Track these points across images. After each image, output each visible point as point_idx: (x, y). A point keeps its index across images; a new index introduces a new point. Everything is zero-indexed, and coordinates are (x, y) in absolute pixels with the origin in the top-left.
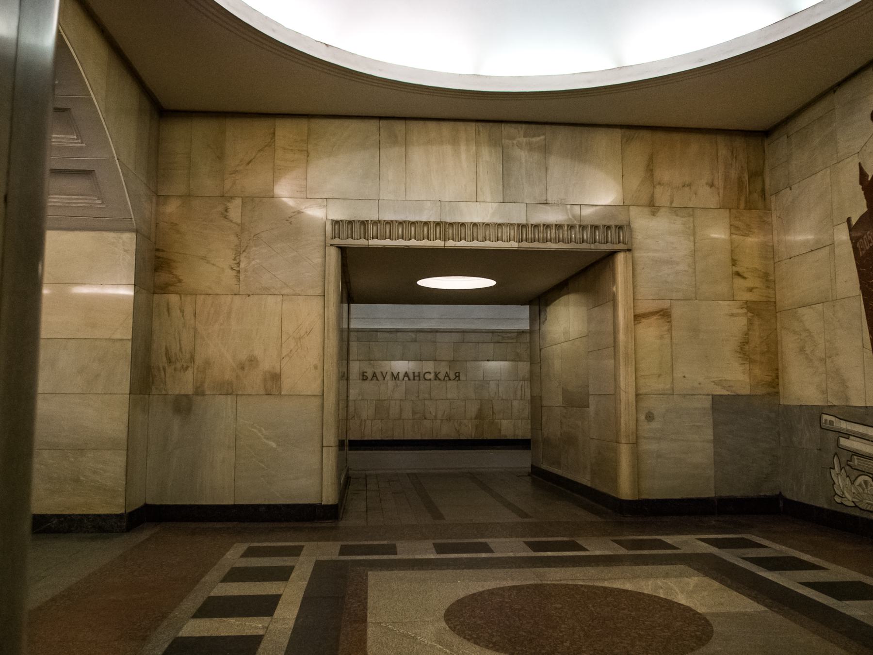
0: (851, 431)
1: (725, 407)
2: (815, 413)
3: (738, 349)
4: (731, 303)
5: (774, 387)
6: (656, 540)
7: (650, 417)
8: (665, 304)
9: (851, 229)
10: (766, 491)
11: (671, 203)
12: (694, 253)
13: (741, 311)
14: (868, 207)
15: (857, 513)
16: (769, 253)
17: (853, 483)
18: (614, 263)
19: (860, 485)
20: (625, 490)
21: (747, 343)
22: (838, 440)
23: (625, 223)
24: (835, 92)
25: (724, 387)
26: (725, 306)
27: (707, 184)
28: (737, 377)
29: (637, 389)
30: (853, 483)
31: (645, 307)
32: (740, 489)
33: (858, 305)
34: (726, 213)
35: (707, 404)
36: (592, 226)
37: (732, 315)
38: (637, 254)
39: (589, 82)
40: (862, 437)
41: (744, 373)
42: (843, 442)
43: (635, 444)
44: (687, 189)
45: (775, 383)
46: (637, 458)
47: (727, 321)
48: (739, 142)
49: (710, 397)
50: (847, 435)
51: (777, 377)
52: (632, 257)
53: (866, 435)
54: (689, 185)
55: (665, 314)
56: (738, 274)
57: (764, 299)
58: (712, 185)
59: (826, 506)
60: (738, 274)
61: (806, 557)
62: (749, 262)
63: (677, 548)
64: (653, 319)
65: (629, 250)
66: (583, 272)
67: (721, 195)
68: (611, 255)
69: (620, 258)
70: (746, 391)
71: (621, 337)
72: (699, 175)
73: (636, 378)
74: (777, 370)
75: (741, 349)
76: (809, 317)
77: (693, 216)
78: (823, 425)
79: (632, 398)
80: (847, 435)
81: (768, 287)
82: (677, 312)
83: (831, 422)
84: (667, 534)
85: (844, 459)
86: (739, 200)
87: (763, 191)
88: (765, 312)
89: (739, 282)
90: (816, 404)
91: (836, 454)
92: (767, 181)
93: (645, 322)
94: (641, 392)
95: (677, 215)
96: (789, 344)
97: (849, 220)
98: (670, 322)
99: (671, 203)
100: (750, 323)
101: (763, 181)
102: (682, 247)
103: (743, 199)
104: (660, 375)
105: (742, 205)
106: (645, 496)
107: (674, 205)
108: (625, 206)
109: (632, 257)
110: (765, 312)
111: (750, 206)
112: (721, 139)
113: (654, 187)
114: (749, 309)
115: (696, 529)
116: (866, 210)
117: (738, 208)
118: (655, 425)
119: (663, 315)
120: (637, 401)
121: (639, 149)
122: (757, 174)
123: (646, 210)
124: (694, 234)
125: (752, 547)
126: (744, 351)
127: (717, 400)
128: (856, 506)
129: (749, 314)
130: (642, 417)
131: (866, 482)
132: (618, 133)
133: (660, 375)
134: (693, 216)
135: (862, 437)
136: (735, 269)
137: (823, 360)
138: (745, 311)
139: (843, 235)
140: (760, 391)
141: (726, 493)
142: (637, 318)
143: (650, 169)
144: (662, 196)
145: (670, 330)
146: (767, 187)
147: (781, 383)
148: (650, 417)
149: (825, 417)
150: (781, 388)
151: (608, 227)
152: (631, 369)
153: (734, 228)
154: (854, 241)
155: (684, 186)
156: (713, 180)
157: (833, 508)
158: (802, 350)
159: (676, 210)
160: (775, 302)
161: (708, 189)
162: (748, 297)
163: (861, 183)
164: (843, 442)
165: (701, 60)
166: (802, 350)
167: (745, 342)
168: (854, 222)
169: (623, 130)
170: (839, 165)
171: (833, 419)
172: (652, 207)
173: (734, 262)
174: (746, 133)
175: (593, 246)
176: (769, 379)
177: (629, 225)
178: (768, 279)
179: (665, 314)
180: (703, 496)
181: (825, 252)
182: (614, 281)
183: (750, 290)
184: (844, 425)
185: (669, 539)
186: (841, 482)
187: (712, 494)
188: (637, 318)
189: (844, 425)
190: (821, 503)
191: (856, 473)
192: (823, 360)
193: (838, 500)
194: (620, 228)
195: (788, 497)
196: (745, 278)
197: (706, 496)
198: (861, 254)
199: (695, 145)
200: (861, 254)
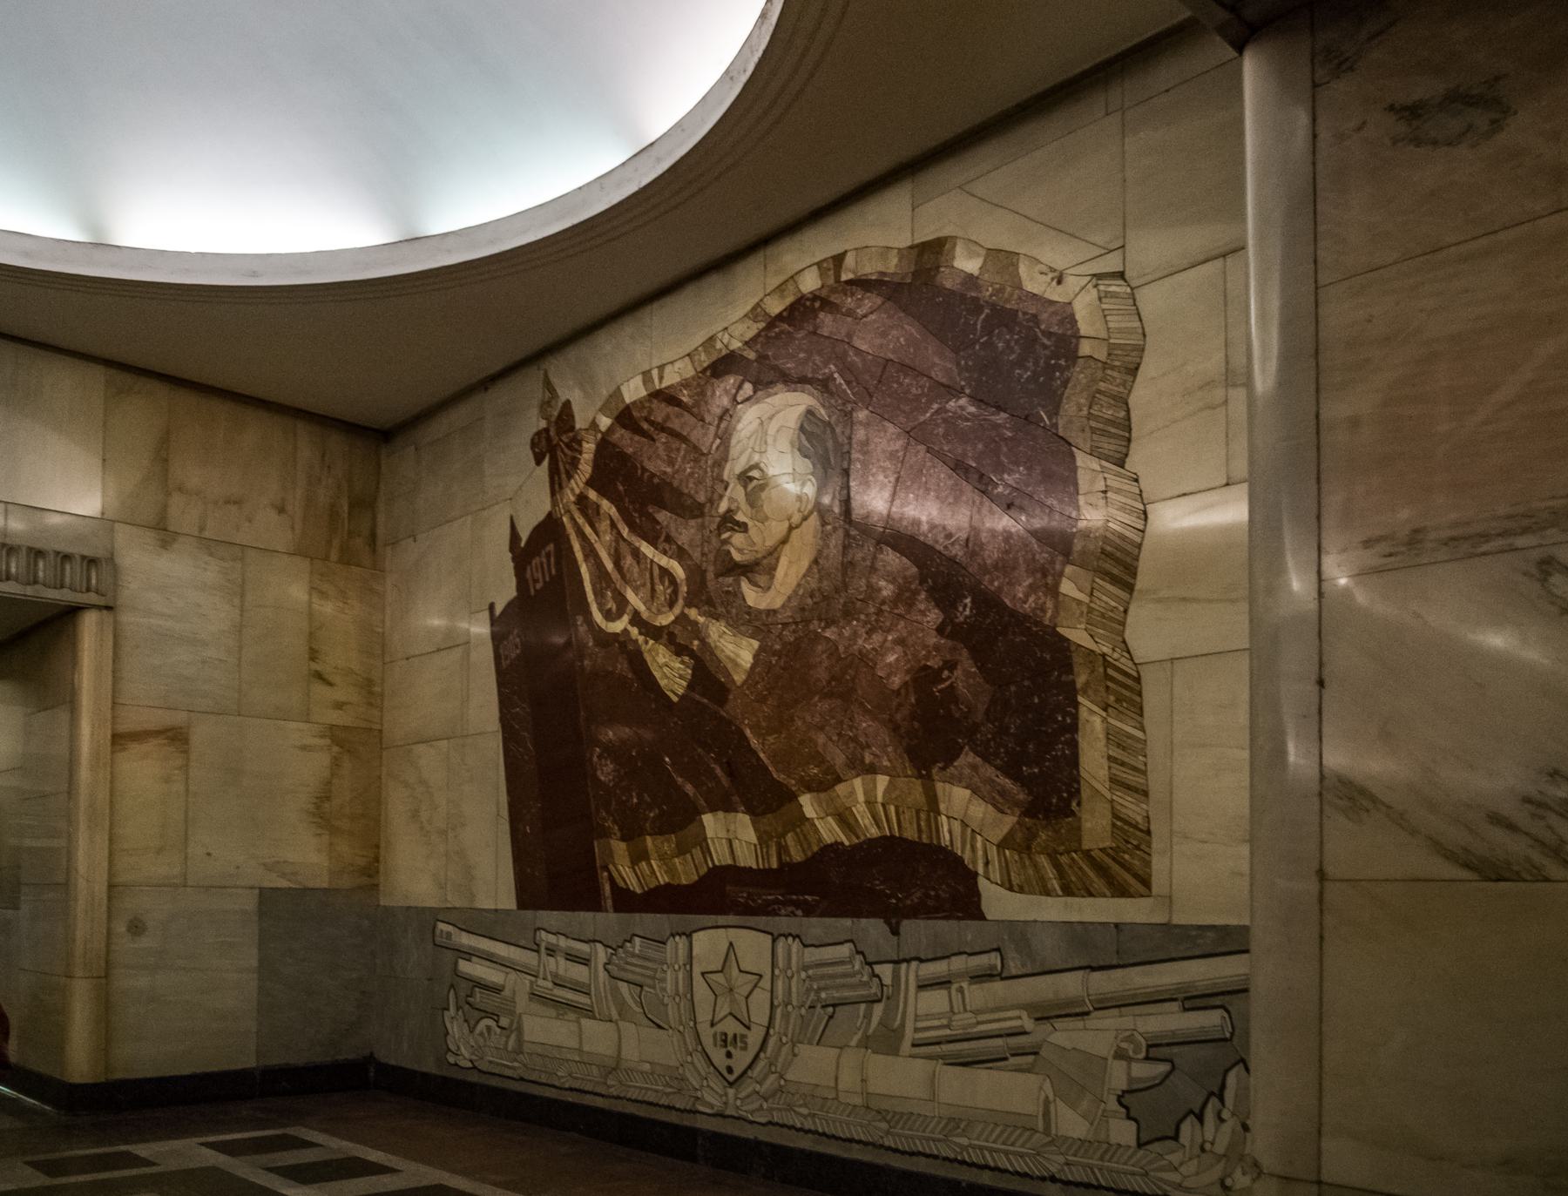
0: (474, 949)
1: (282, 909)
2: (427, 918)
3: (311, 807)
4: (302, 725)
5: (370, 876)
6: (122, 1153)
7: (137, 927)
8: (179, 718)
9: (494, 621)
10: (347, 1054)
11: (202, 529)
12: (239, 629)
13: (318, 741)
14: (518, 589)
15: (474, 1078)
16: (377, 646)
17: (472, 1031)
18: (75, 626)
19: (481, 1034)
20: (79, 1061)
21: (328, 798)
22: (456, 964)
23: (100, 553)
24: (486, 389)
25: (283, 875)
26: (297, 732)
27: (273, 506)
28: (308, 857)
29: (111, 873)
30: (472, 1031)
31: (132, 720)
32: (299, 1052)
33: (494, 746)
34: (303, 565)
35: (250, 903)
36: (30, 549)
37: (304, 748)
38: (126, 618)
39: (27, 254)
40: (490, 958)
41: (319, 851)
42: (464, 966)
43: (104, 975)
44: (233, 508)
45: (371, 871)
46: (105, 1005)
47: (297, 758)
48: (336, 442)
49: (257, 892)
50: (469, 954)
51: (377, 860)
52: (115, 622)
53: (493, 954)
54: (238, 502)
55: (177, 737)
56: (319, 676)
57: (363, 725)
58: (281, 510)
59: (434, 1071)
60: (319, 676)
61: (375, 1156)
62: (341, 656)
63: (154, 1164)
64: (150, 746)
65: (109, 608)
66: (21, 637)
67: (298, 531)
68: (70, 613)
69: (89, 623)
70: (323, 882)
71: (84, 774)
72: (257, 485)
73: (111, 854)
74: (378, 847)
75: (318, 807)
76: (429, 760)
77: (242, 559)
78: (438, 940)
79: (101, 889)
80: (469, 954)
81: (370, 704)
82: (201, 734)
83: (449, 935)
84: (136, 1142)
85: (462, 994)
86: (329, 542)
87: (373, 536)
88: (361, 746)
89: (319, 689)
90: (428, 905)
91: (452, 986)
92: (381, 518)
93: (135, 748)
94: (120, 879)
95: (211, 555)
96: (397, 804)
97: (492, 607)
98: (186, 752)
99: (202, 529)
100: (336, 763)
101: (374, 518)
102: (217, 616)
103: (336, 543)
104: (160, 851)
105: (334, 556)
106: (119, 1075)
107: (206, 534)
108: (106, 522)
109: (115, 622)
110: (361, 746)
111: (347, 558)
112: (302, 427)
113: (168, 494)
114: (336, 741)
115: (176, 1130)
116: (514, 594)
117: (327, 558)
118: (145, 942)
119: (173, 739)
120: (110, 898)
121: (143, 413)
122: (364, 504)
123: (150, 536)
124: (242, 596)
125: (297, 1148)
126: (322, 814)
127: (267, 897)
128: (475, 1067)
129: (336, 749)
130: (120, 928)
131: (489, 1028)
132: (98, 374)
133: (160, 851)
134: (242, 559)
135: (490, 958)
136: (314, 666)
137: (443, 833)
138: (328, 741)
139: (480, 629)
140: (346, 882)
141: (276, 1059)
142: (119, 740)
143: (162, 457)
144: (183, 515)
145: (185, 768)
146: (381, 531)
147: (381, 868)
148: (137, 927)
149: (441, 926)
150: (382, 879)
151: (67, 557)
152: (102, 839)
153: (313, 589)
154: (497, 639)
155: (227, 502)
156: (283, 499)
157: (445, 1073)
158: (415, 814)
159: (209, 545)
160: (381, 731)
161: (273, 515)
162: (334, 717)
163: (511, 550)
164: (464, 966)
165: (254, 274)
166: (415, 814)
167: (324, 796)
168: (498, 610)
169: (112, 372)
170: (485, 513)
171: (450, 928)
172: (164, 533)
173: (313, 655)
174: (353, 429)
175: (29, 591)
176: (361, 862)
177: (111, 559)
178: (371, 691)
179: (177, 737)
180: (233, 1067)
181: (456, 654)
182: (75, 662)
183: (339, 706)
184: (466, 940)
185: (142, 1150)
186: (456, 1029)
187: (251, 1063)
188: (119, 740)
189: (466, 940)
190: (429, 1066)
191: (477, 1014)
192: (443, 833)
193: (452, 1059)
194: (92, 562)
195: (383, 1060)
196: (330, 684)
197: (240, 1066)
198: (505, 664)
199: (255, 431)
200: (505, 664)
